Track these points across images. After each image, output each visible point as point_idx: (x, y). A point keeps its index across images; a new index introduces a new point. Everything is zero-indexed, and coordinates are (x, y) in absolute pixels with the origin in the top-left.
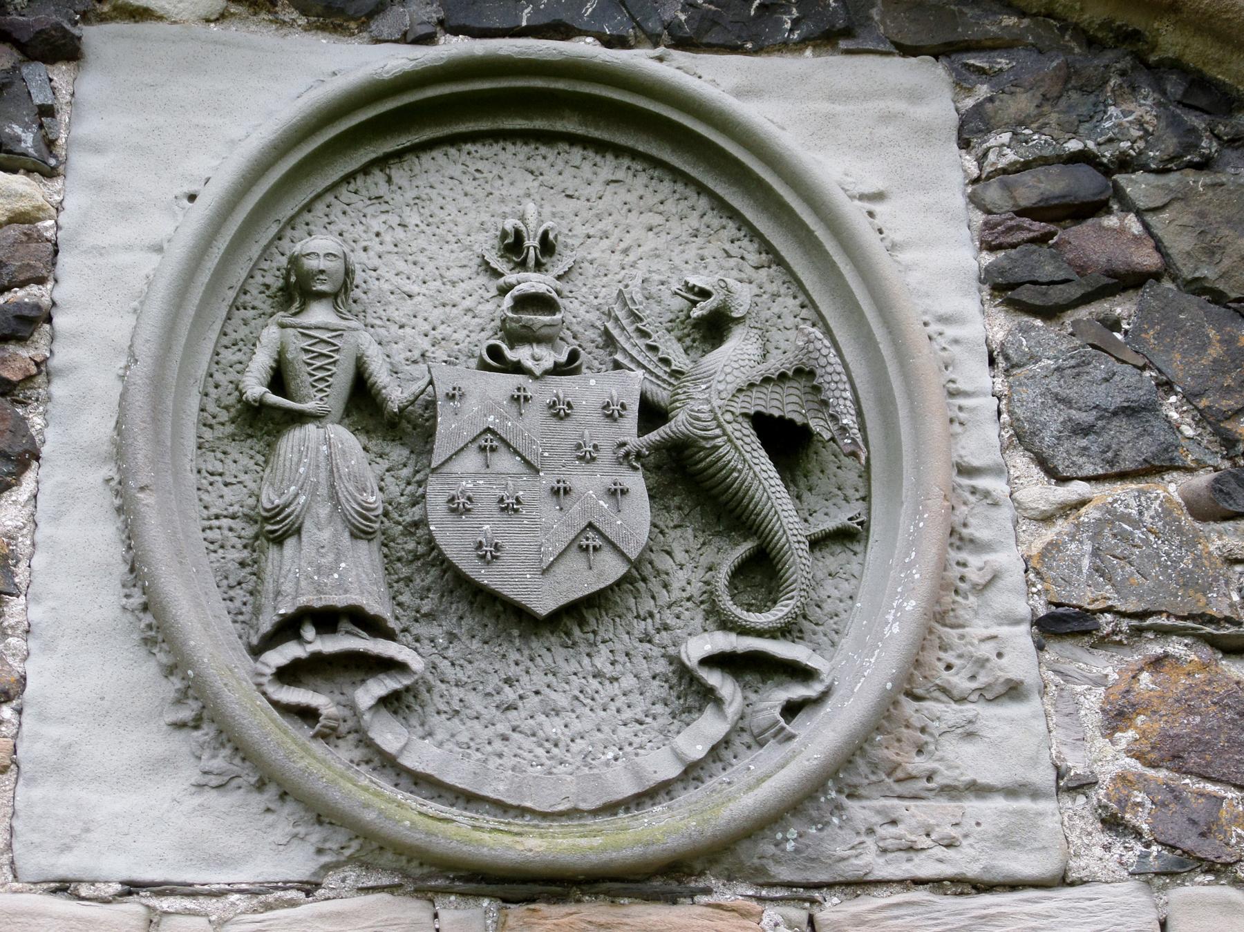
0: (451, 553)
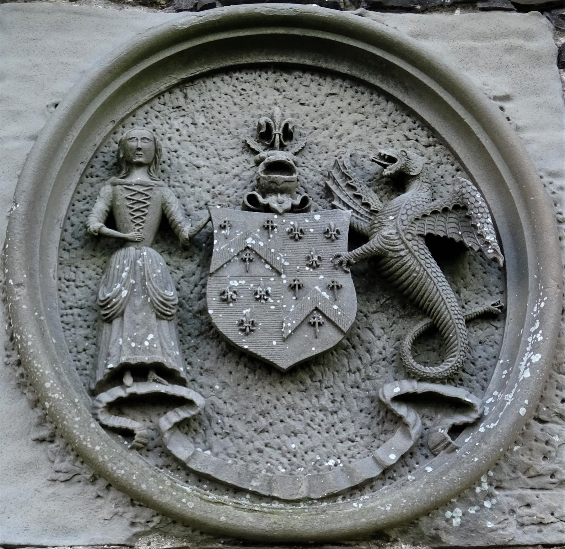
0: (221, 328)
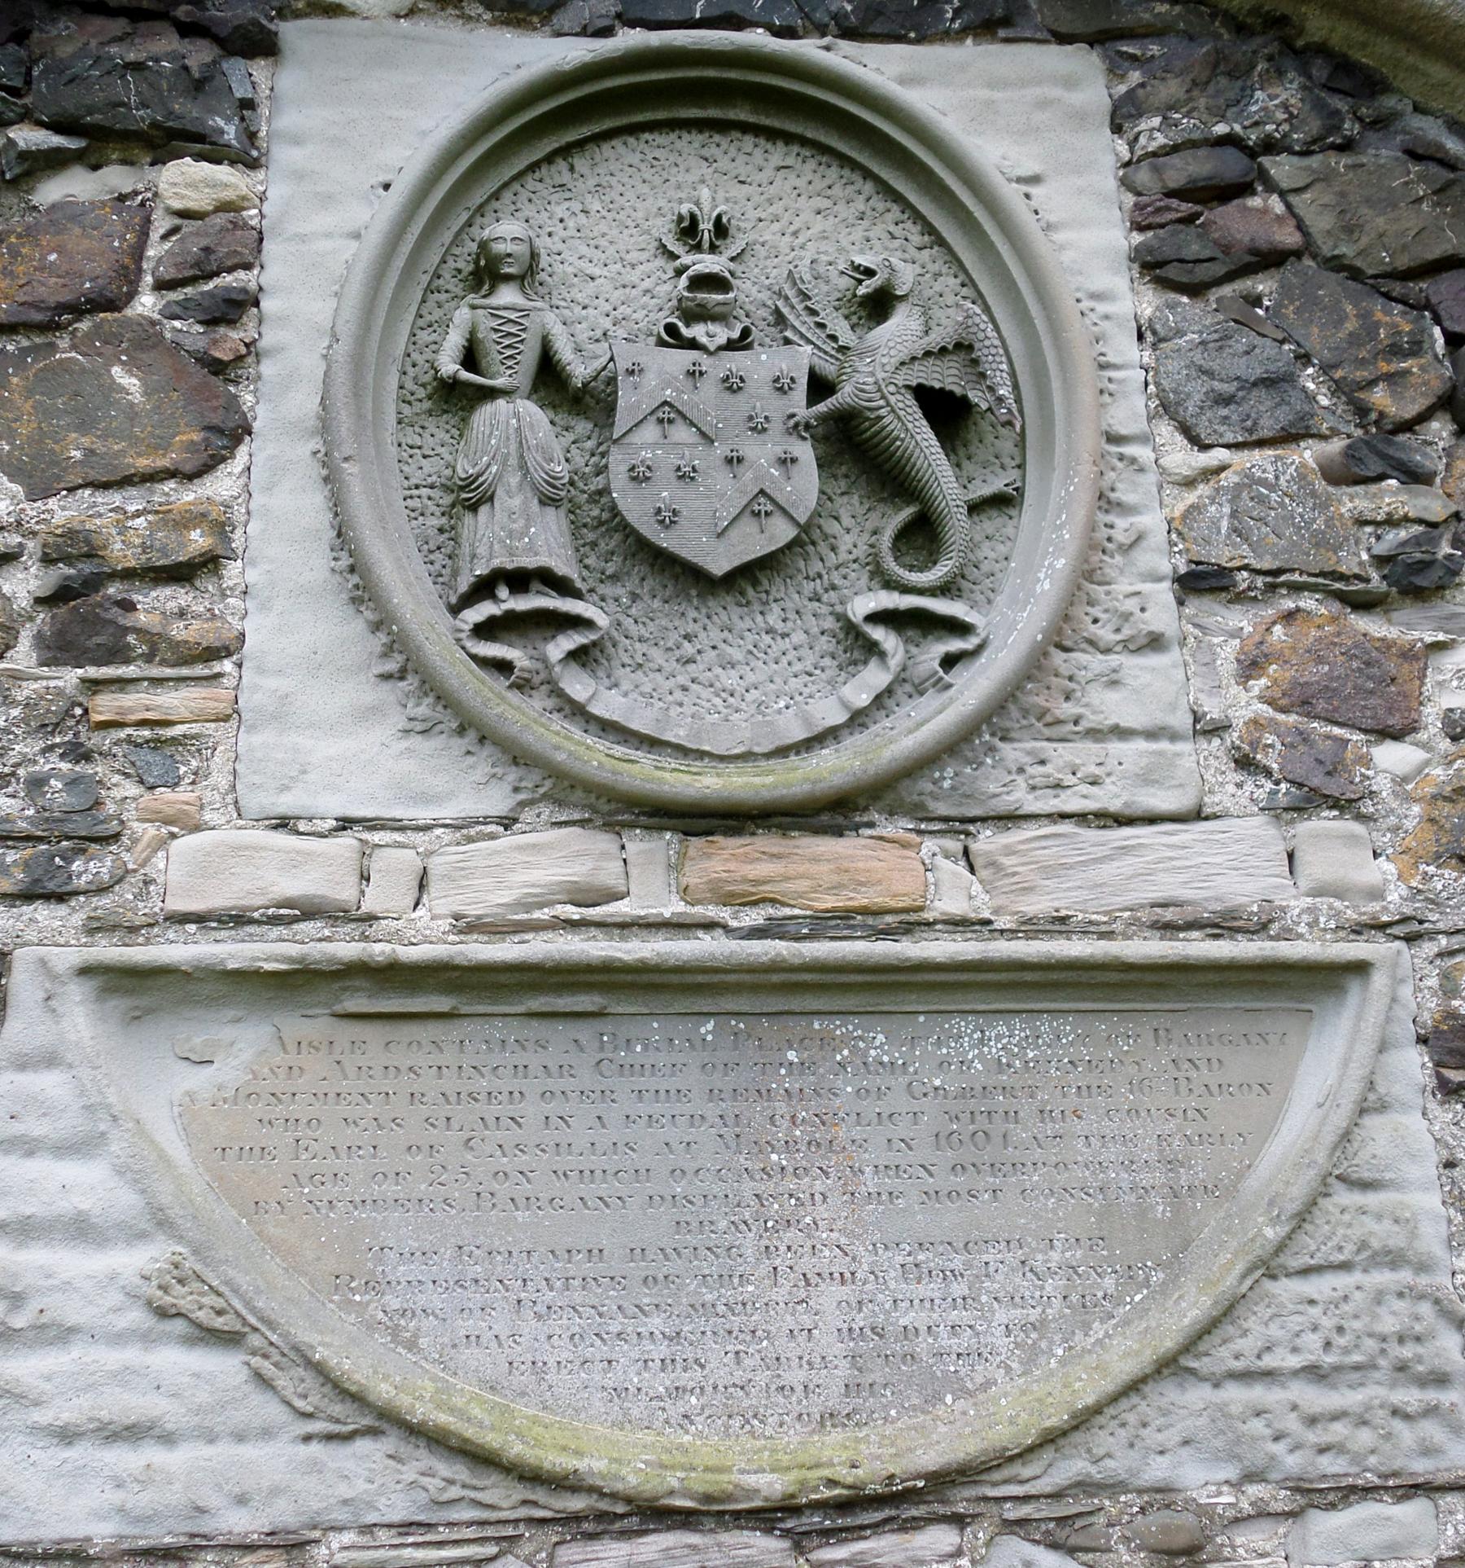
0: (632, 518)
